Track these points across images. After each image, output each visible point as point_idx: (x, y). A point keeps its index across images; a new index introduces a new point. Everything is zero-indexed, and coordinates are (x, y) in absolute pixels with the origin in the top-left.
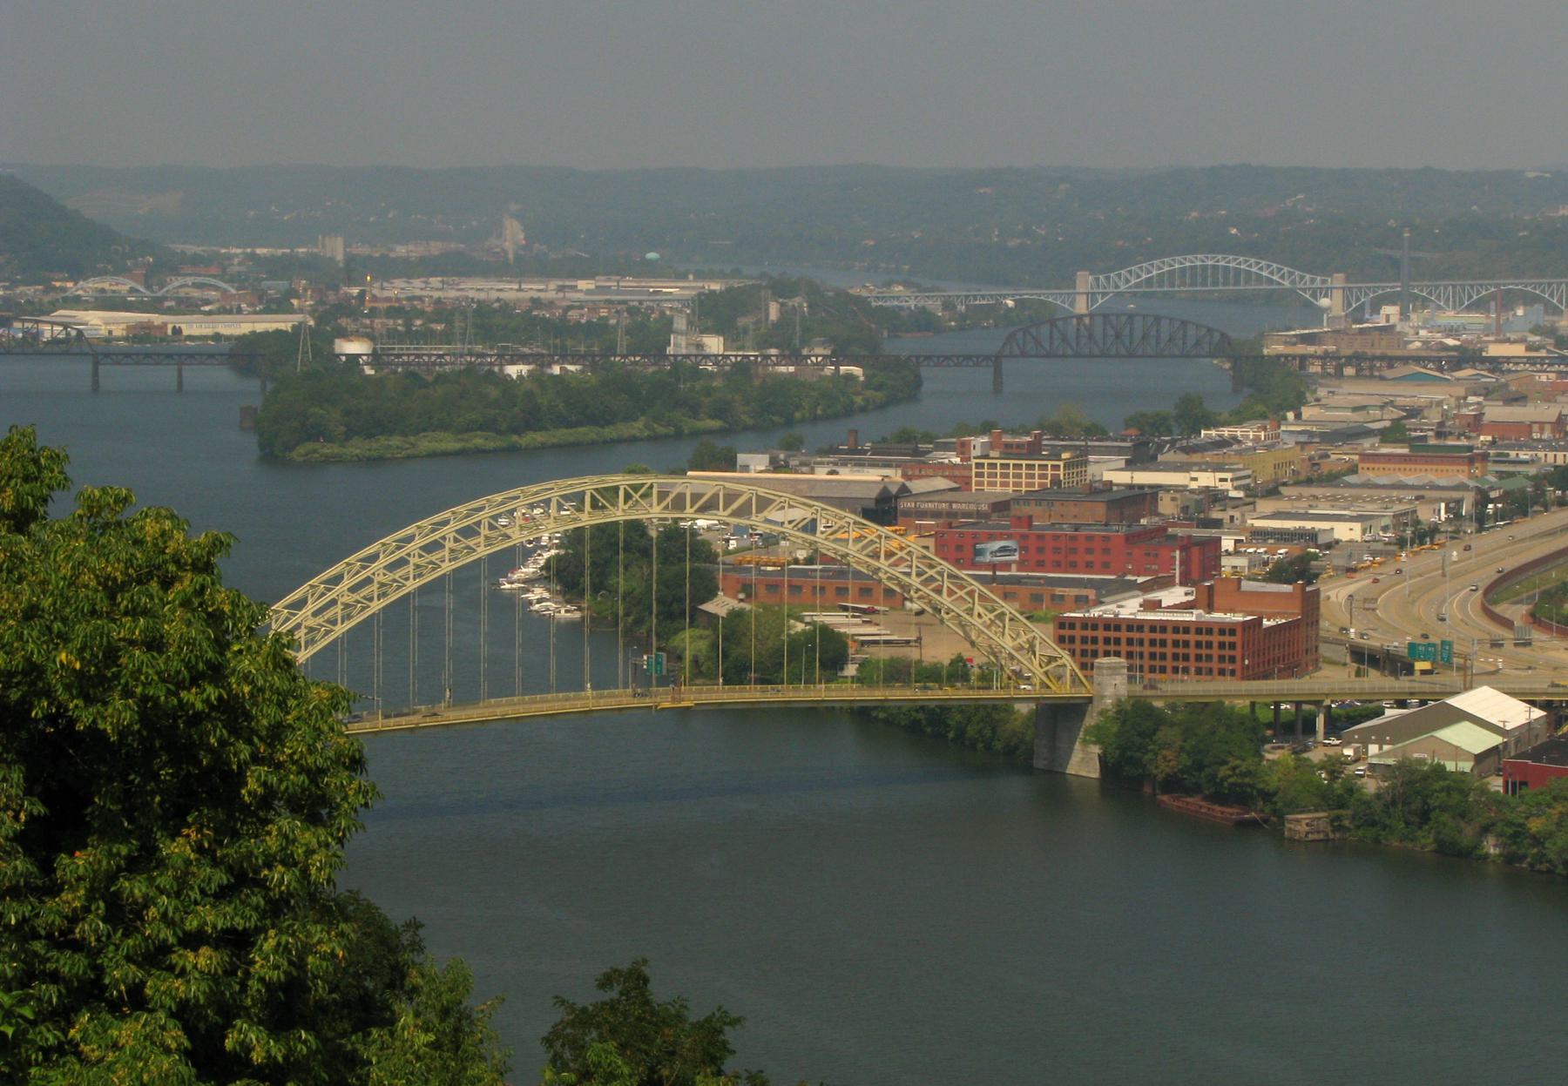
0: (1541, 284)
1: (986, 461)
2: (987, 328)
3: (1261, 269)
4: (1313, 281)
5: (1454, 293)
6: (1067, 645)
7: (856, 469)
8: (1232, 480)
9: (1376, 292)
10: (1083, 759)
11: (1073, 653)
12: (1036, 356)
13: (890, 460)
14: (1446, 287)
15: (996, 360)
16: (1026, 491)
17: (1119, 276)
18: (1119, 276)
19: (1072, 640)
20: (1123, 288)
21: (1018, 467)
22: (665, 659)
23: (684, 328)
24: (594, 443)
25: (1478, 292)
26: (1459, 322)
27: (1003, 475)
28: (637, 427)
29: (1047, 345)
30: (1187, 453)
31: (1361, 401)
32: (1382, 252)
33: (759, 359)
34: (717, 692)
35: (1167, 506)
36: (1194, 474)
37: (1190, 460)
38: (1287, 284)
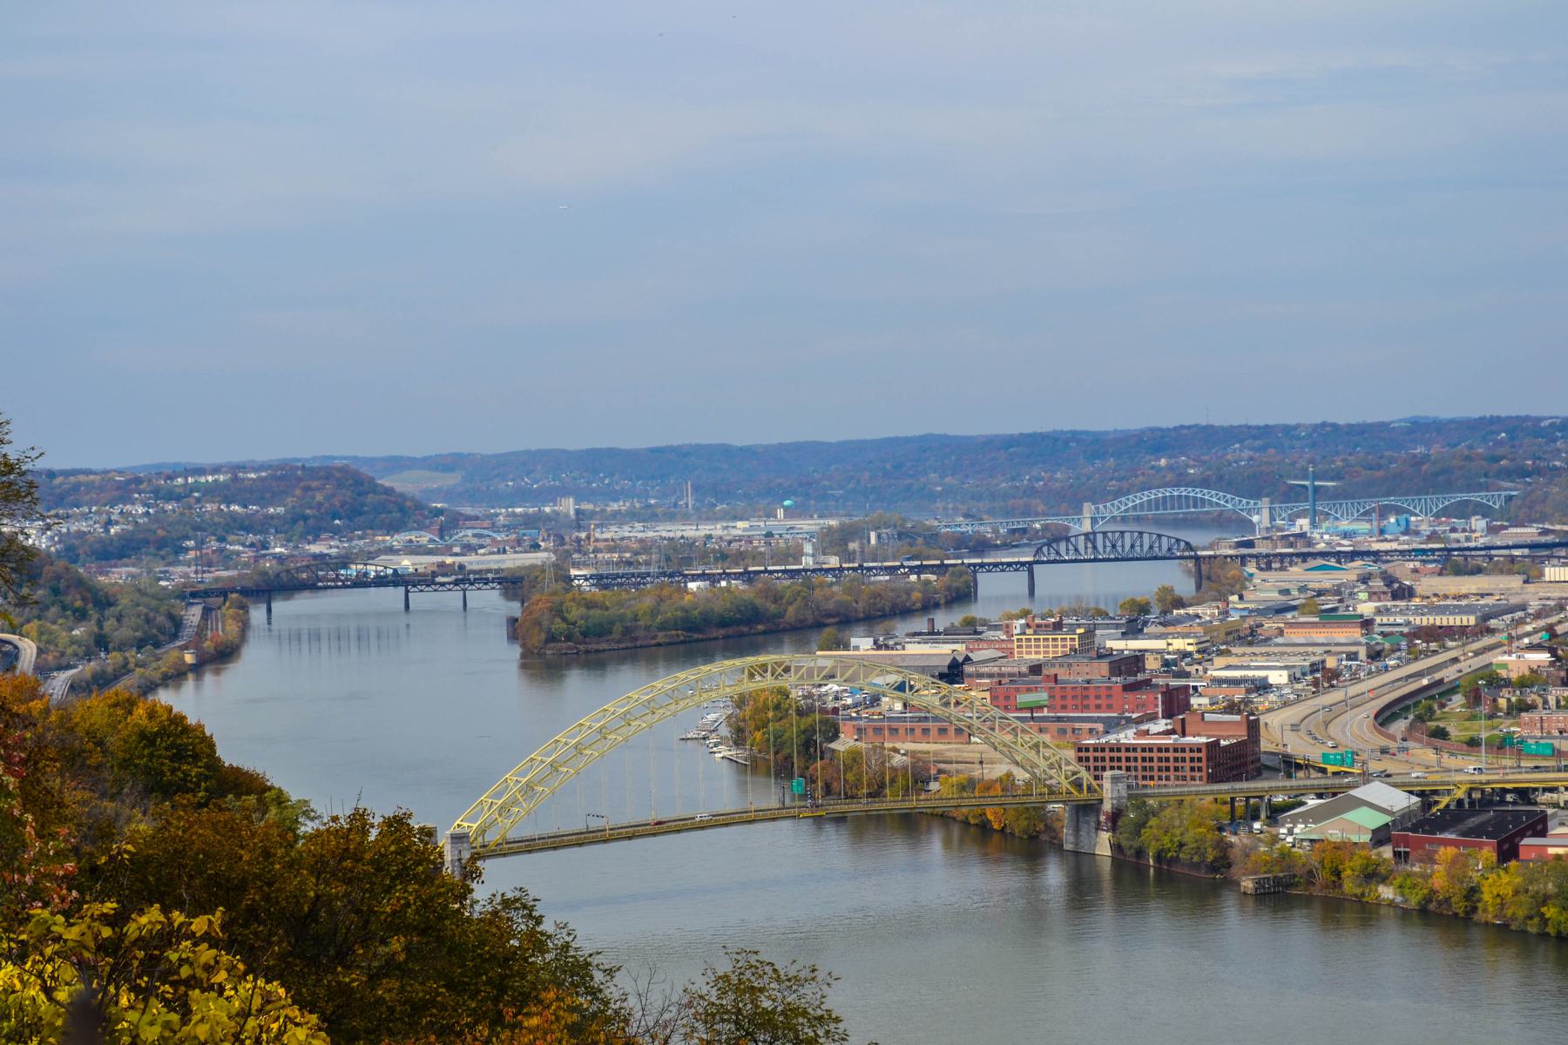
1: (1024, 637)
4: (1248, 503)
5: (1426, 504)
6: (1085, 764)
11: (1088, 769)
14: (1420, 500)
19: (1087, 759)
20: (1116, 514)
27: (1027, 647)
30: (1165, 626)
36: (1170, 641)
38: (1230, 506)
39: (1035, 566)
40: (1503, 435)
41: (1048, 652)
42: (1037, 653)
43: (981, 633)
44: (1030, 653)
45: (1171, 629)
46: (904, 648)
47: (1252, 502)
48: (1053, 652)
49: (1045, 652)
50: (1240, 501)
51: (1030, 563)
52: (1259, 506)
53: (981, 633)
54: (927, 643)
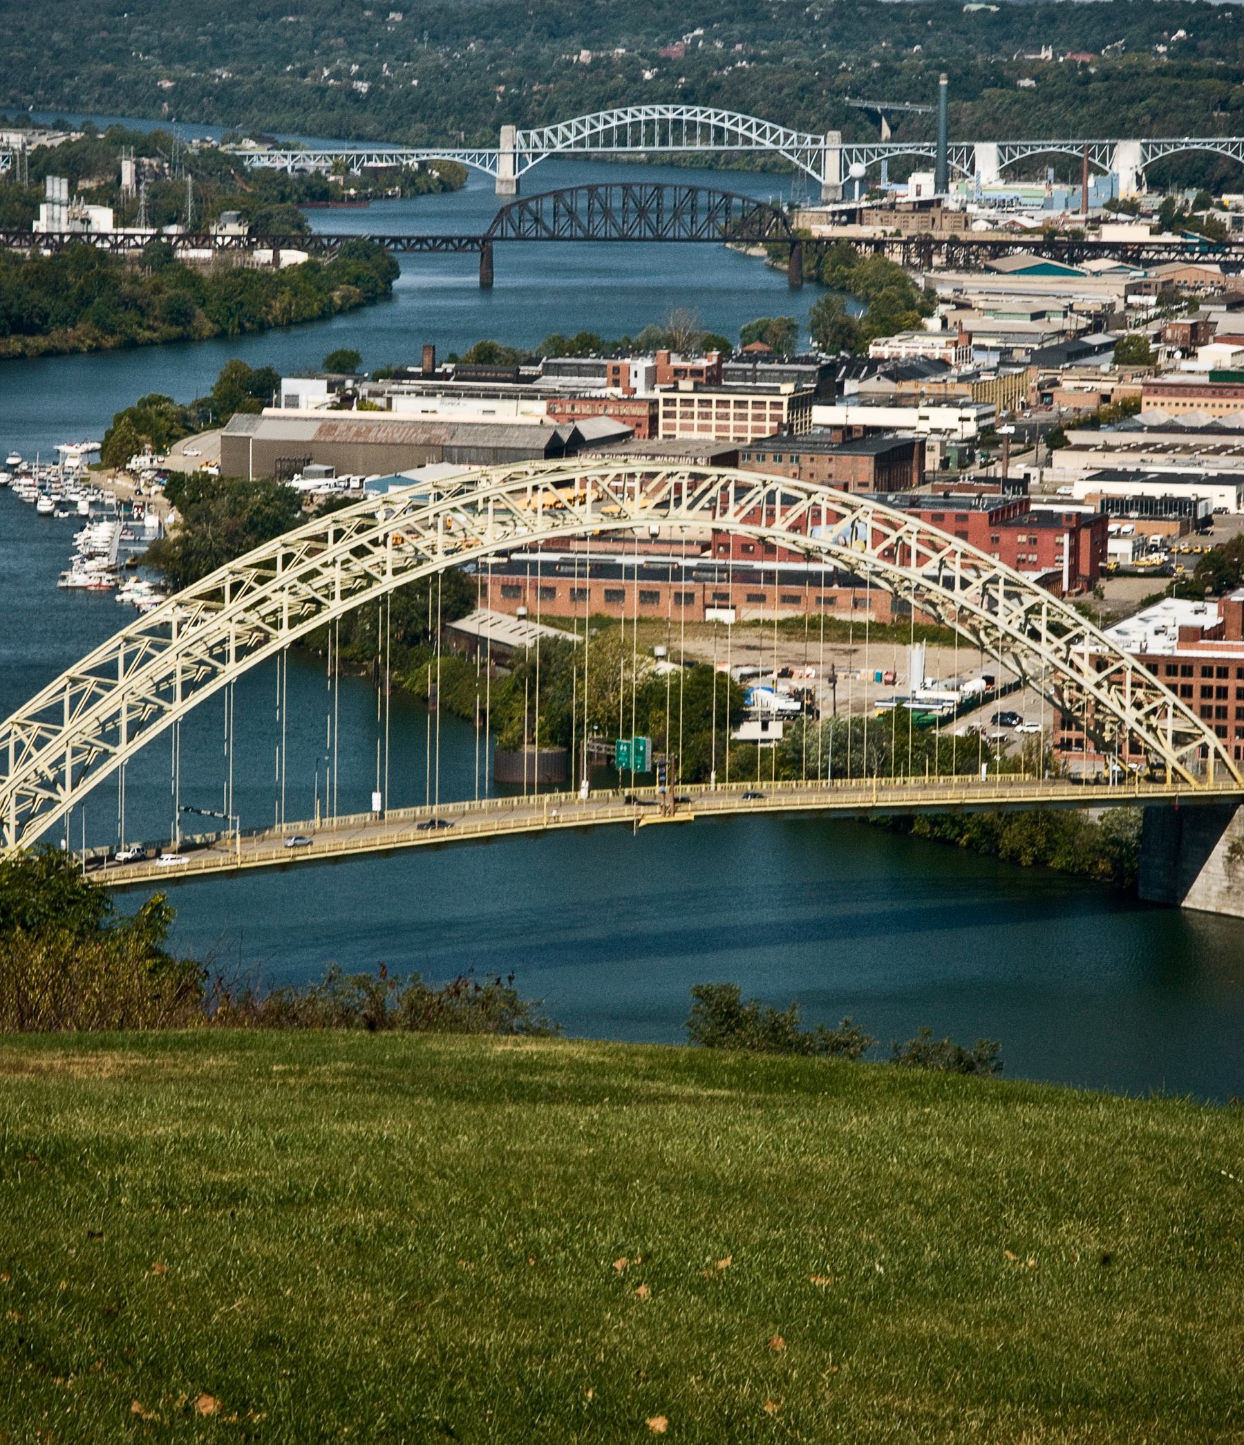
0: (480, 155)
2: (393, 197)
3: (722, 120)
4: (801, 140)
7: (448, 400)
8: (978, 419)
9: (1165, 150)
10: (1229, 888)
12: (571, 239)
13: (494, 389)
15: (484, 245)
16: (755, 440)
17: (555, 132)
18: (555, 132)
20: (559, 148)
21: (725, 403)
22: (649, 747)
23: (64, 196)
24: (22, 356)
25: (1154, 154)
26: (1012, 195)
28: (81, 333)
29: (549, 222)
30: (896, 381)
31: (1039, 304)
32: (859, 103)
33: (66, 239)
34: (710, 795)
35: (342, 427)
37: (900, 391)
38: (768, 145)
39: (496, 245)
40: (1181, 33)
41: (726, 428)
42: (703, 428)
43: (531, 379)
44: (690, 428)
45: (908, 387)
46: (389, 406)
47: (809, 137)
48: (755, 430)
49: (719, 428)
50: (787, 136)
51: (487, 239)
52: (821, 145)
53: (531, 379)
54: (434, 395)
